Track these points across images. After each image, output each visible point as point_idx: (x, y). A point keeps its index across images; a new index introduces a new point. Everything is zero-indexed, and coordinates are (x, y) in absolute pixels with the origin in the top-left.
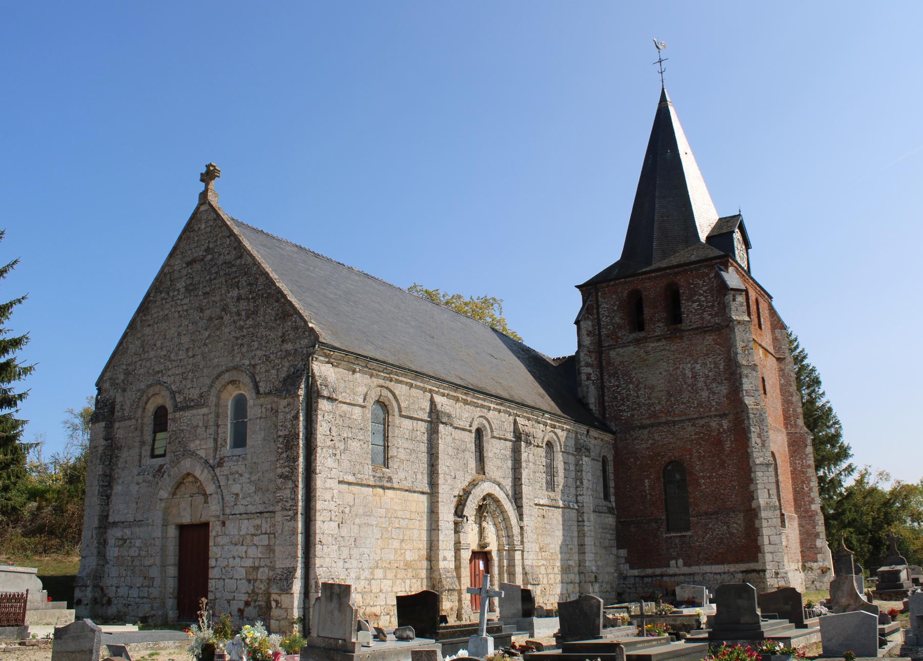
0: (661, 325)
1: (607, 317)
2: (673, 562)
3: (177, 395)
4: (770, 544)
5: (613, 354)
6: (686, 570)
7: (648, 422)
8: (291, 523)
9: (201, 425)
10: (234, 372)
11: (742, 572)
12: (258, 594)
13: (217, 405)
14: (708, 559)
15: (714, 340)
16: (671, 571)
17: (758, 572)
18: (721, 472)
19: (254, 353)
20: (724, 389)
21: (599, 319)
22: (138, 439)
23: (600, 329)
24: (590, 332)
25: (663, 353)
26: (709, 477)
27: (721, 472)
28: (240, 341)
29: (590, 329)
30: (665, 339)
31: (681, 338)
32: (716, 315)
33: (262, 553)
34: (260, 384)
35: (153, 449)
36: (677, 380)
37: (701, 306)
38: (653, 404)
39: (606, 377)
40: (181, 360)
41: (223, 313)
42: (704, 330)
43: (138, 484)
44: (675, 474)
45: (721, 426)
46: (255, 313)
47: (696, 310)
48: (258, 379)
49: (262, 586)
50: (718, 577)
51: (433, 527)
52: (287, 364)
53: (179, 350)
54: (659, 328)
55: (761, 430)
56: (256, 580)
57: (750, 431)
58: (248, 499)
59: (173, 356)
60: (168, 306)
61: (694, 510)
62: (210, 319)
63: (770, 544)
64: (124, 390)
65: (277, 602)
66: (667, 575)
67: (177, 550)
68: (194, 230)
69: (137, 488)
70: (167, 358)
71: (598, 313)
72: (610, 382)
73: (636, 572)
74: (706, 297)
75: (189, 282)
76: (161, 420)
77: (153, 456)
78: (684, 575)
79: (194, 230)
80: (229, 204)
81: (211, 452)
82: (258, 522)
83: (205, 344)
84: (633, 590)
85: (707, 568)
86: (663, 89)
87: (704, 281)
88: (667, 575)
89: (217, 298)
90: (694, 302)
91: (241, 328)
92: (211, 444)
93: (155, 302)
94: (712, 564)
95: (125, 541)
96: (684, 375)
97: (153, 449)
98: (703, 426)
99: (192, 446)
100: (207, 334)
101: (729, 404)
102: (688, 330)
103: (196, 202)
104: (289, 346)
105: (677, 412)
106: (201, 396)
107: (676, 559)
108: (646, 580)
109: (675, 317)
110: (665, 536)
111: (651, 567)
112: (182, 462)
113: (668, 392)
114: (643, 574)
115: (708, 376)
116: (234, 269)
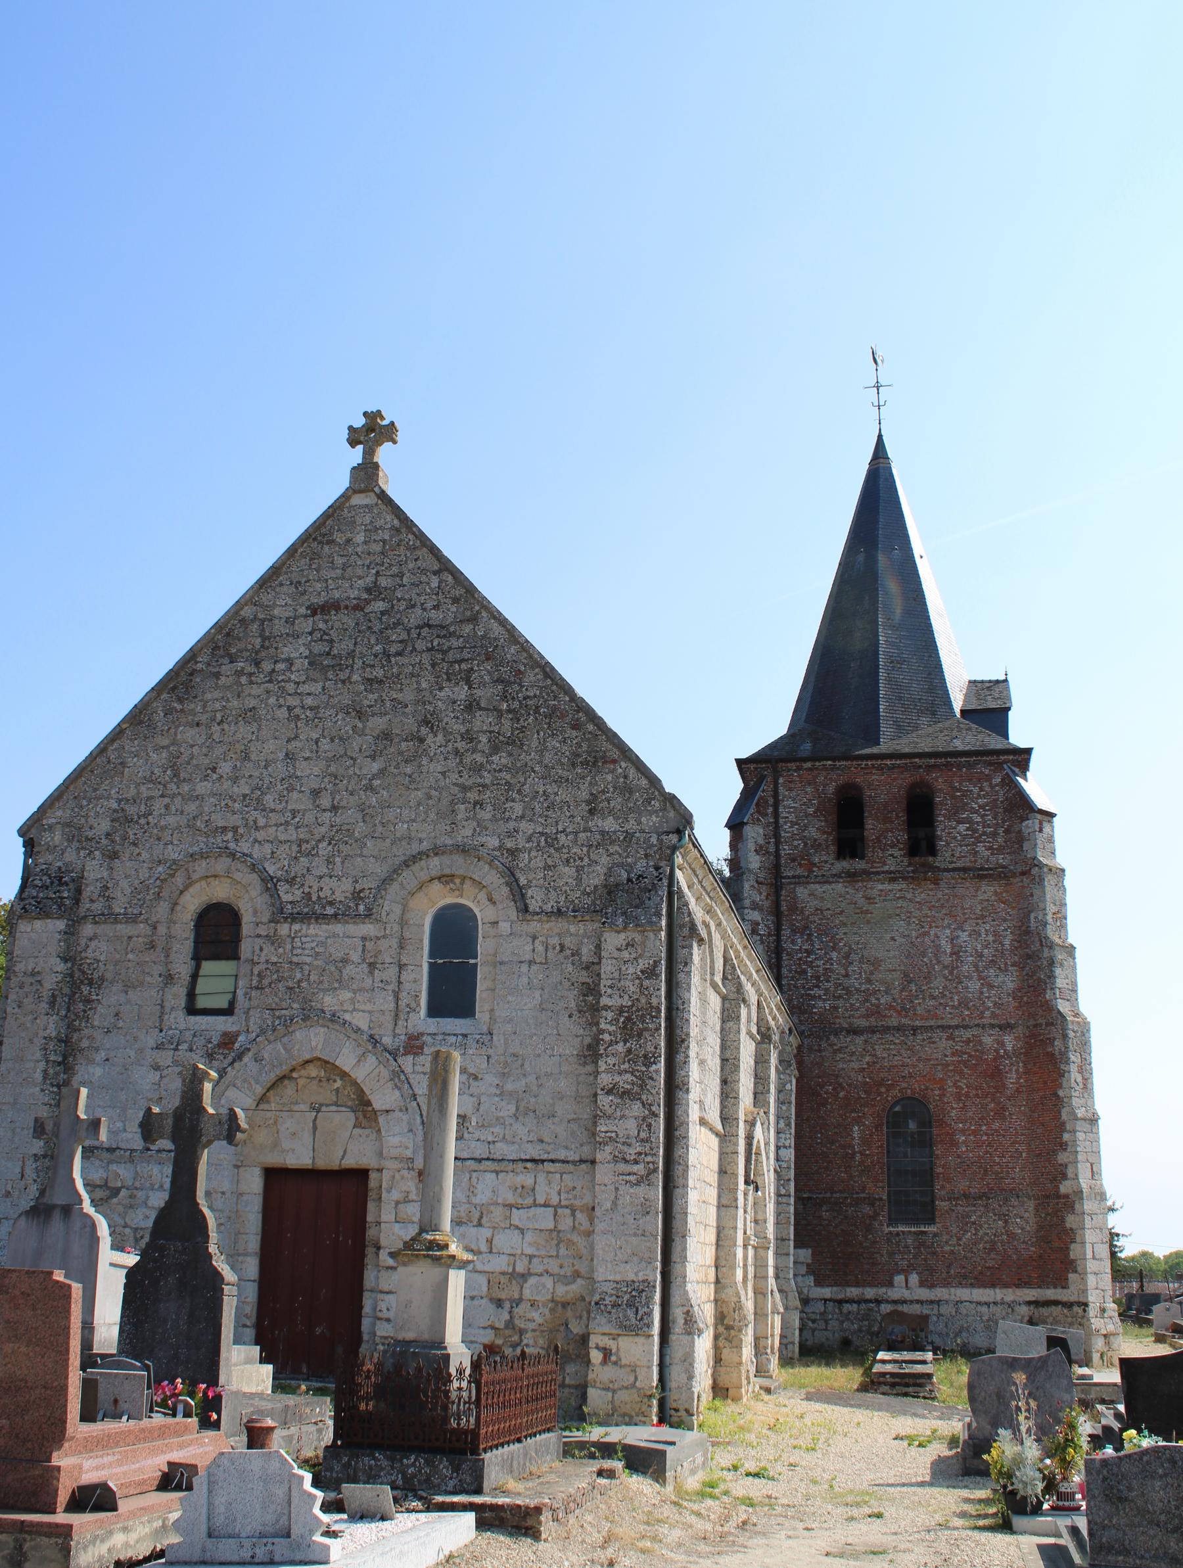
0: (897, 853)
1: (793, 824)
2: (899, 1279)
3: (283, 888)
4: (1094, 1258)
5: (802, 892)
6: (924, 1294)
7: (863, 1023)
8: (641, 1191)
9: (355, 957)
10: (459, 859)
11: (1029, 1303)
12: (521, 1332)
13: (403, 923)
14: (965, 1277)
15: (996, 893)
16: (895, 1293)
17: (1069, 1305)
18: (996, 1125)
19: (512, 825)
20: (1009, 982)
21: (777, 827)
22: (157, 969)
23: (777, 843)
24: (761, 847)
25: (900, 903)
26: (975, 1133)
27: (996, 1125)
28: (472, 796)
29: (761, 841)
30: (904, 879)
31: (936, 882)
32: (1000, 850)
33: (535, 1244)
34: (530, 893)
35: (191, 995)
36: (924, 955)
37: (975, 831)
38: (875, 992)
39: (786, 932)
40: (294, 813)
41: (424, 730)
42: (981, 874)
43: (156, 1068)
44: (912, 1124)
45: (1002, 1044)
46: (515, 742)
47: (965, 837)
48: (523, 881)
49: (535, 1315)
50: (984, 1309)
51: (724, 1201)
52: (605, 860)
53: (291, 789)
54: (894, 859)
55: (1084, 1059)
56: (519, 1302)
57: (1067, 1062)
58: (497, 1130)
59: (269, 800)
60: (255, 690)
61: (943, 1187)
62: (386, 736)
63: (1094, 1258)
64: (114, 856)
65: (607, 1353)
66: (887, 1302)
67: (260, 1224)
68: (331, 542)
69: (154, 1076)
70: (254, 800)
71: (776, 814)
72: (793, 942)
73: (827, 1292)
74: (983, 816)
75: (319, 648)
76: (218, 932)
77: (192, 1010)
78: (918, 1301)
79: (331, 542)
80: (403, 476)
81: (388, 1019)
82: (528, 1180)
83: (370, 788)
84: (822, 1325)
85: (964, 1293)
86: (880, 437)
87: (981, 789)
88: (887, 1302)
89: (408, 695)
90: (959, 822)
91: (477, 769)
92: (386, 1002)
93: (217, 675)
94: (972, 1286)
95: (116, 1192)
96: (938, 947)
97: (191, 995)
98: (968, 1041)
99: (329, 1002)
100: (376, 767)
101: (1017, 1008)
102: (948, 870)
103: (342, 483)
104: (609, 824)
105: (919, 1010)
106: (357, 896)
107: (906, 1272)
108: (847, 1307)
109: (921, 841)
110: (886, 1230)
111: (857, 1284)
112: (298, 1035)
113: (906, 975)
114: (840, 1296)
115: (981, 956)
116: (455, 643)
